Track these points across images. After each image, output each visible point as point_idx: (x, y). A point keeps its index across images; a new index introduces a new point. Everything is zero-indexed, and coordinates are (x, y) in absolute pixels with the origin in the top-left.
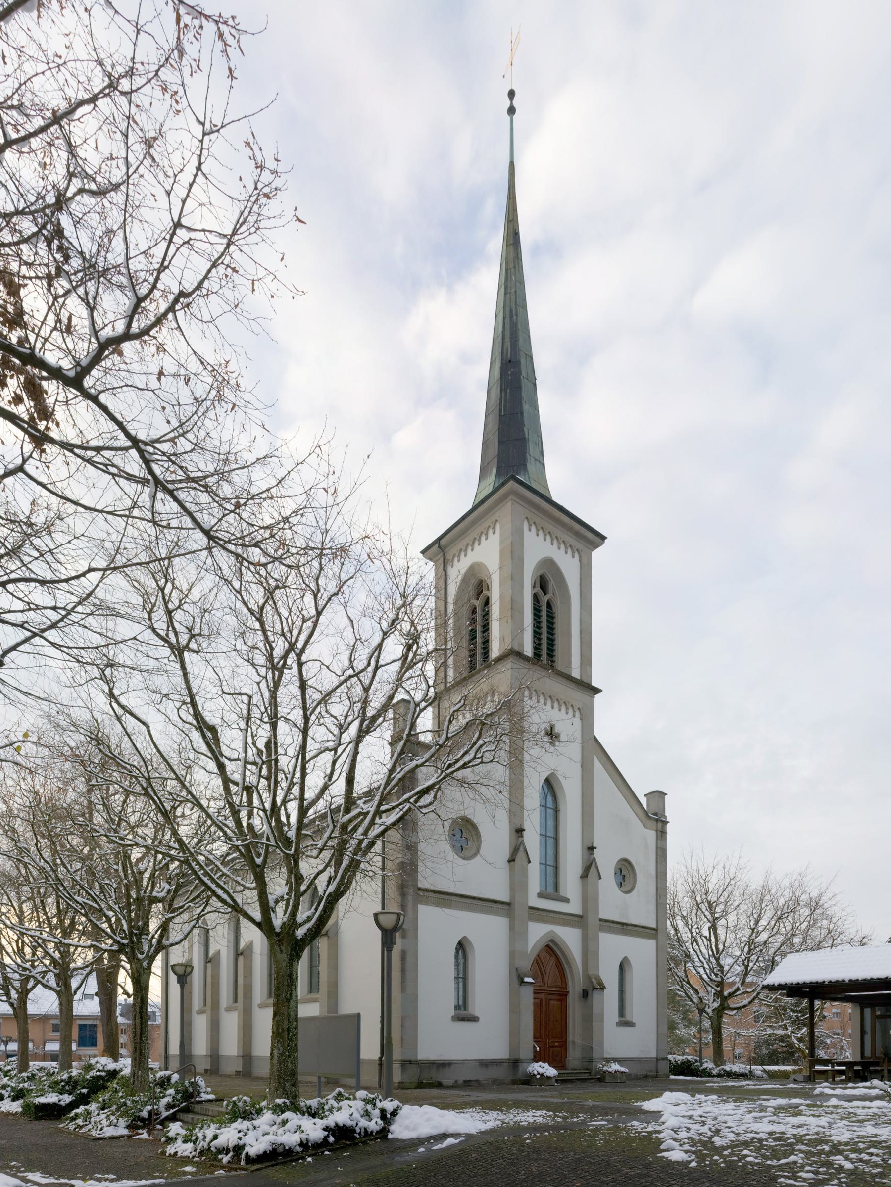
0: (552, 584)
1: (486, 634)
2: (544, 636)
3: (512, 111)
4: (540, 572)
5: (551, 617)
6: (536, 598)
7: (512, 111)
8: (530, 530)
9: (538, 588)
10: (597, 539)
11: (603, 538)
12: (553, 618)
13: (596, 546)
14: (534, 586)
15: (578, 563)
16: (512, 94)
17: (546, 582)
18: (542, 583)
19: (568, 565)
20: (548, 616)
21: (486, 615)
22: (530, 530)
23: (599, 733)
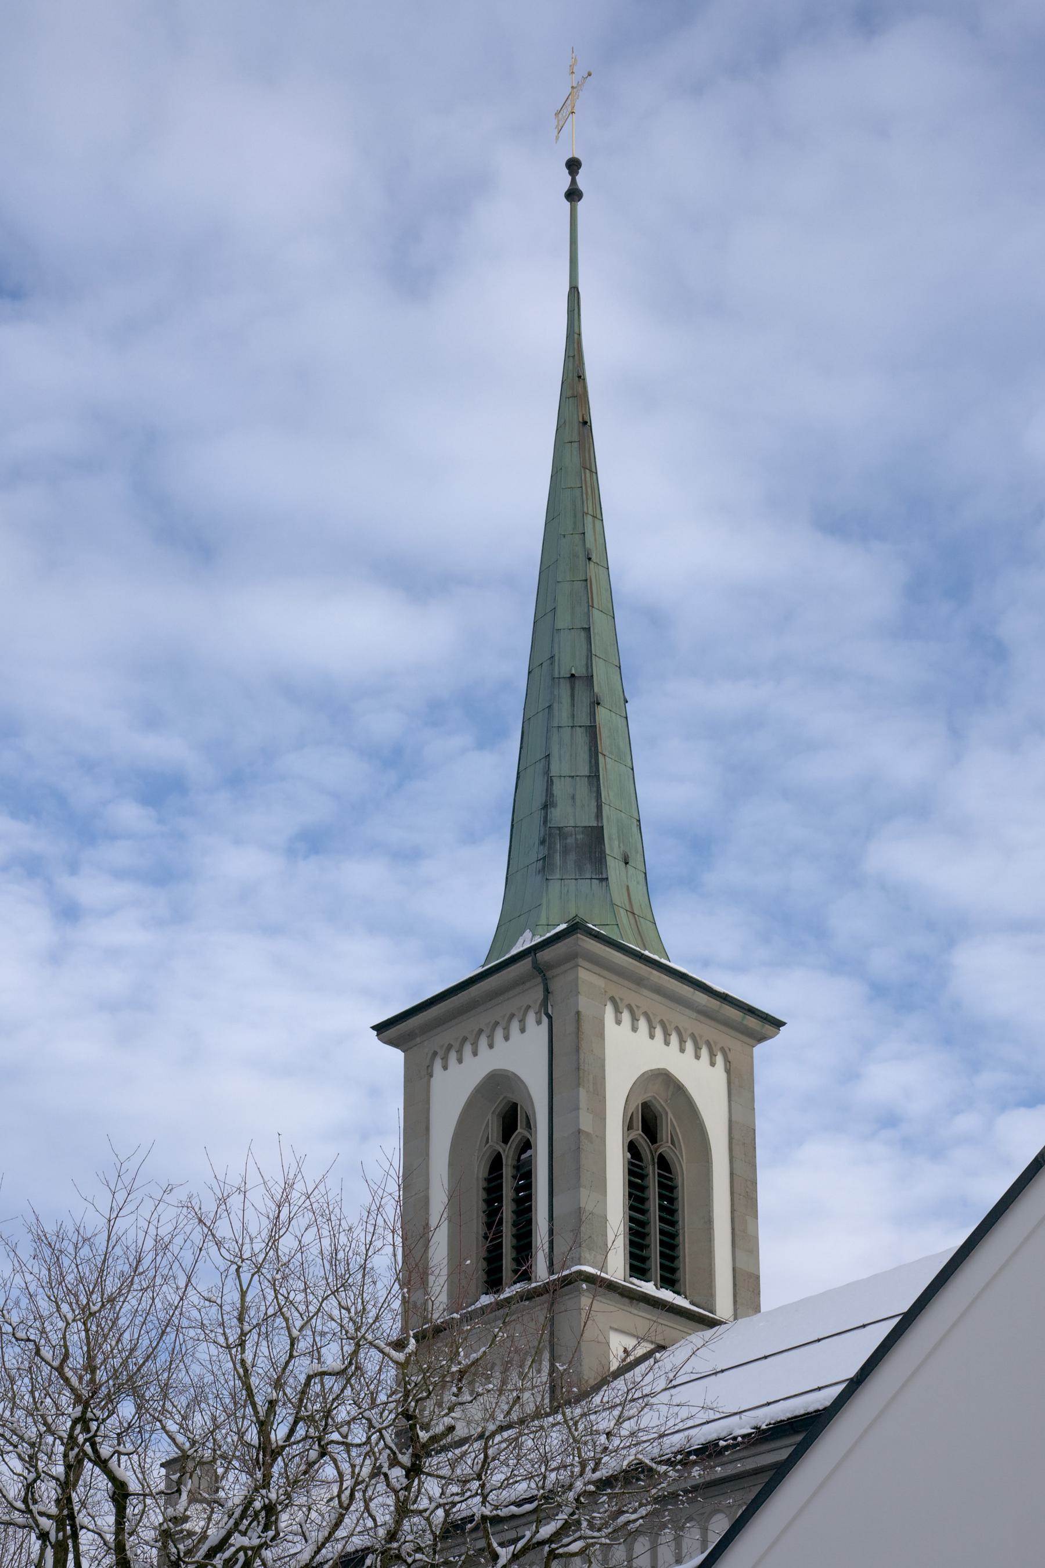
0: (670, 1123)
1: (559, 903)
2: (655, 1227)
3: (573, 195)
4: (645, 1097)
5: (668, 1190)
6: (632, 1148)
7: (573, 195)
8: (618, 1022)
9: (637, 1133)
10: (768, 1028)
11: (778, 1024)
12: (672, 1189)
13: (762, 1039)
14: (630, 1127)
15: (723, 1076)
16: (573, 166)
17: (657, 1128)
18: (647, 1122)
19: (704, 1082)
20: (661, 1185)
21: (525, 1174)
22: (618, 1022)
23: (570, 178)
